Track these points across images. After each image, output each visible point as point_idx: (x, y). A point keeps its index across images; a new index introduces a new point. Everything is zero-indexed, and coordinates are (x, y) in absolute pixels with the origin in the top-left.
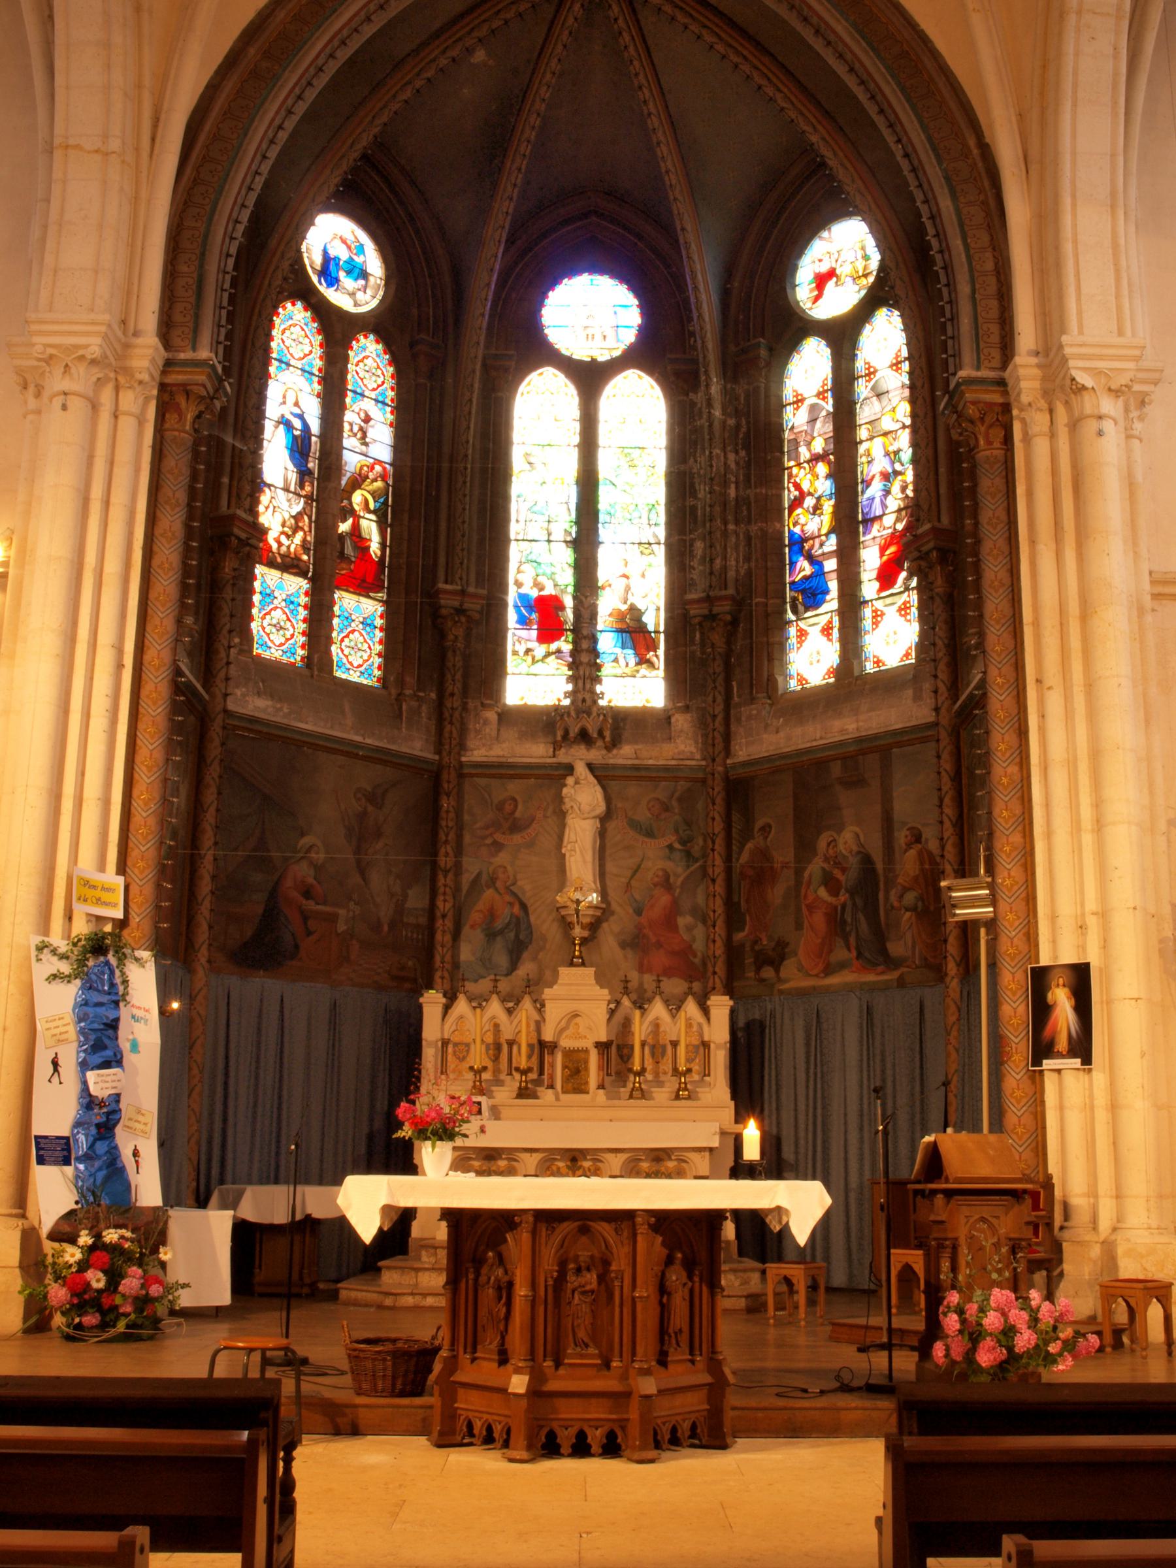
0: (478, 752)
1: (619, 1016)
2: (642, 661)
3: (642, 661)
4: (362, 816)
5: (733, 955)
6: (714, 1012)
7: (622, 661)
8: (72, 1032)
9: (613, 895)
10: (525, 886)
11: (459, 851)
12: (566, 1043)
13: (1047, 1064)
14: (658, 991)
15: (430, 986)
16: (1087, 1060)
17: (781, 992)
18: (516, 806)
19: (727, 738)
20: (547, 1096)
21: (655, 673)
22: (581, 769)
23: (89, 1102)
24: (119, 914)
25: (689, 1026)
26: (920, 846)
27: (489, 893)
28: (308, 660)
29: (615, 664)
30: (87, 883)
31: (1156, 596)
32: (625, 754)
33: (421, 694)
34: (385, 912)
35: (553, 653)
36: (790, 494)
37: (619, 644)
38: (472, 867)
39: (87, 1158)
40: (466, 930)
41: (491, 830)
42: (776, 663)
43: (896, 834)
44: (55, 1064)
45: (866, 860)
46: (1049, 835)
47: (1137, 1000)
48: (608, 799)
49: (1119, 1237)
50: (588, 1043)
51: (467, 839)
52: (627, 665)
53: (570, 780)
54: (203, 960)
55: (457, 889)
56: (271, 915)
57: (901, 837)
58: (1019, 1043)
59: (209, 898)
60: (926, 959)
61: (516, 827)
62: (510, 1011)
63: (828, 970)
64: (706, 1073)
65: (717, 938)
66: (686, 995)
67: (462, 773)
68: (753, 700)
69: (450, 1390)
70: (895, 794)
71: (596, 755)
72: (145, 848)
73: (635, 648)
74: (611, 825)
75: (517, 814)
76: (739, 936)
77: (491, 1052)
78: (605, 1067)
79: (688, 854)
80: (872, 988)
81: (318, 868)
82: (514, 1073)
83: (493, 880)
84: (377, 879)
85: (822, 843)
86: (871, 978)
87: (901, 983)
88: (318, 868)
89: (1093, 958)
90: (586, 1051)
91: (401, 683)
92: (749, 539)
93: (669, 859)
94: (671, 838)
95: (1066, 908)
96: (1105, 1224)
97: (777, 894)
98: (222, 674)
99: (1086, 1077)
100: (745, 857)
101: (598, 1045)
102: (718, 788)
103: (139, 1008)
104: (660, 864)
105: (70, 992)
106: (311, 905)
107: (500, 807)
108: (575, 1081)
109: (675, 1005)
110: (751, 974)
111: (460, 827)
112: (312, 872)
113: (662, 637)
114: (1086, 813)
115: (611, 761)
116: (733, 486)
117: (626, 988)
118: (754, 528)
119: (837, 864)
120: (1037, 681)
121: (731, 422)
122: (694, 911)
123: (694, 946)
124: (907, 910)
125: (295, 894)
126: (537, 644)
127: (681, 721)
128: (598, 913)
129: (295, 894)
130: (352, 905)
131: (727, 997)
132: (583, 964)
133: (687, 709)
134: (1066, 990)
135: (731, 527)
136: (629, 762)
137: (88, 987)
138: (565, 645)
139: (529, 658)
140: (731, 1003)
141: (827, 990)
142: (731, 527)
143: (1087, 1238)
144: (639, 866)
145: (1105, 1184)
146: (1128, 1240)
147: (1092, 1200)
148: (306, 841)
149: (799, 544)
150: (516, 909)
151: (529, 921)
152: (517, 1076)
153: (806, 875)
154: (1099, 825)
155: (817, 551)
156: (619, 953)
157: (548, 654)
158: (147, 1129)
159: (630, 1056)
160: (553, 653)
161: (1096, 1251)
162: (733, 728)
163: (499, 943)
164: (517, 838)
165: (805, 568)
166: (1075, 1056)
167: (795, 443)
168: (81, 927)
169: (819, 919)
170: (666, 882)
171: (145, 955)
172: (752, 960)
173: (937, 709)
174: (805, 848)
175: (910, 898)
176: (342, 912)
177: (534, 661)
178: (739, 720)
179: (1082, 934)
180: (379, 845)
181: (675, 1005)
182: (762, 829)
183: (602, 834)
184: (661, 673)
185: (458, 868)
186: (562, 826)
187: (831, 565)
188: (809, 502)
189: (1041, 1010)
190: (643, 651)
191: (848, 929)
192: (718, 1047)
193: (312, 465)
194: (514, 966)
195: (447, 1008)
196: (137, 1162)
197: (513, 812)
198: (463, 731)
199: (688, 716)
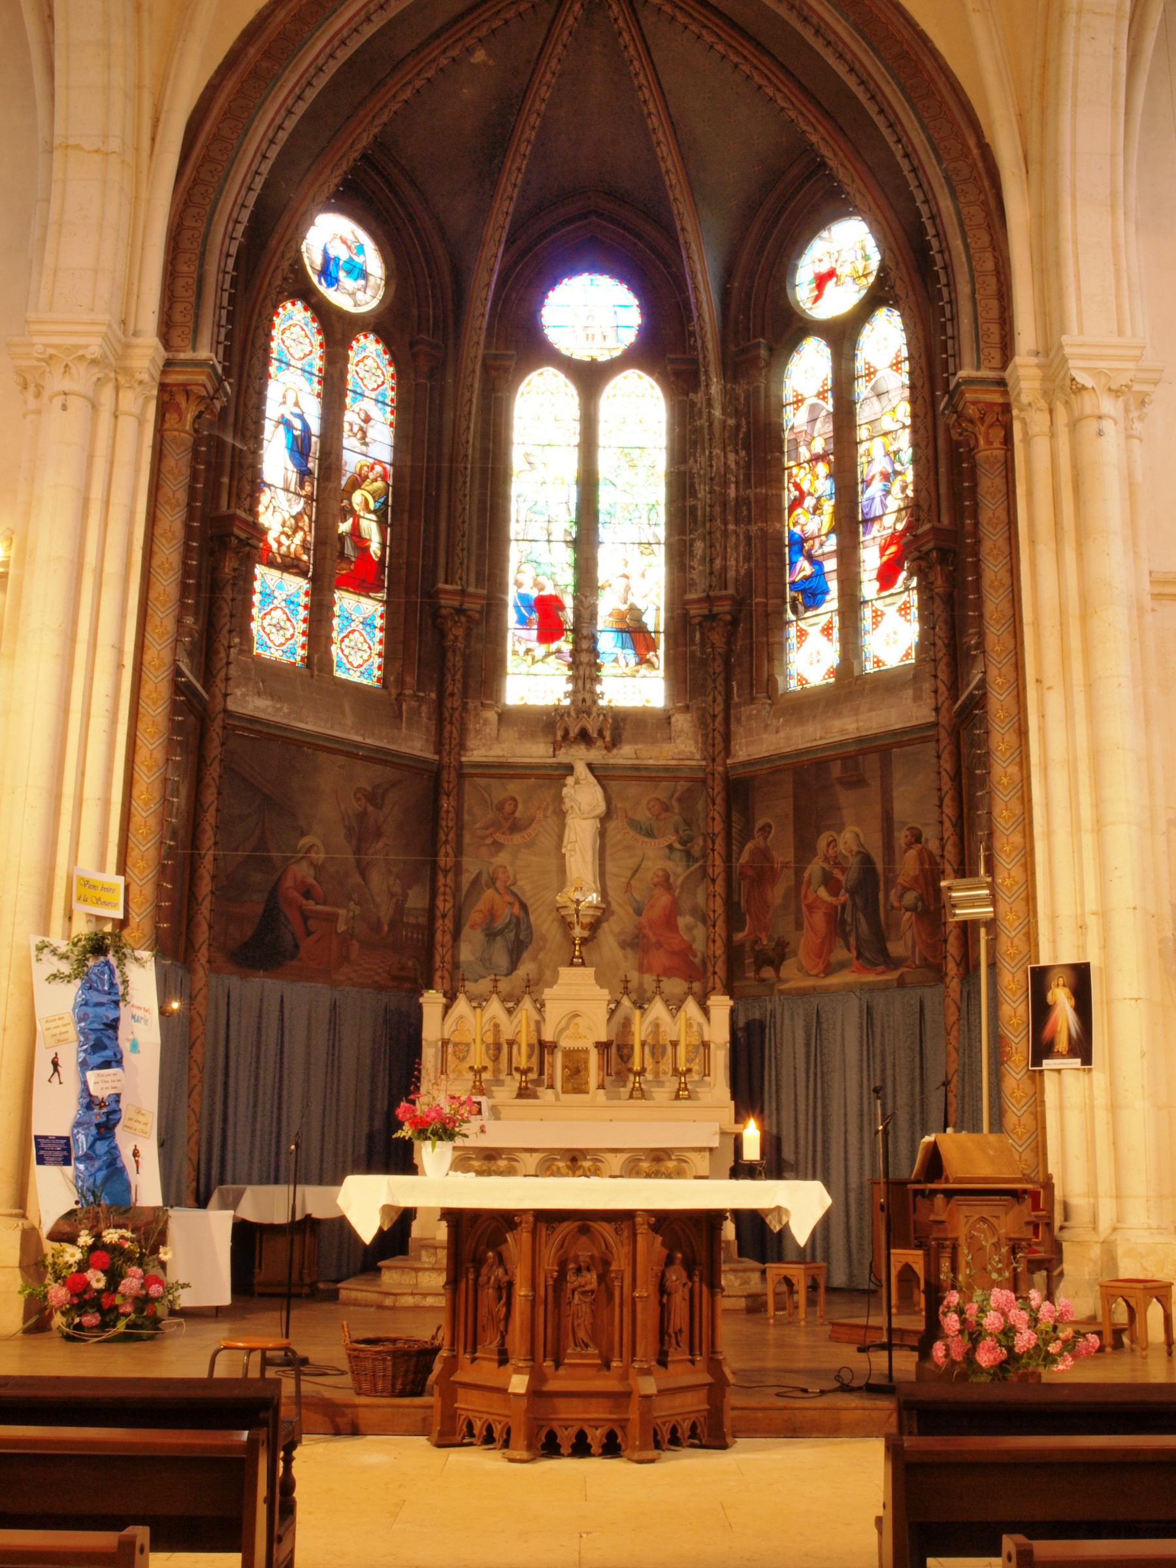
0: (478, 752)
1: (619, 1016)
2: (643, 661)
3: (643, 661)
4: (362, 816)
5: (734, 955)
6: (714, 1012)
7: (622, 662)
8: (72, 1031)
9: (612, 894)
10: (525, 887)
11: (459, 851)
12: (566, 1043)
13: (1047, 1064)
14: (658, 991)
15: (430, 986)
16: (1087, 1060)
17: (781, 992)
18: (516, 806)
19: (727, 738)
20: (547, 1095)
21: (655, 673)
22: (581, 770)
23: (90, 1102)
24: (119, 914)
25: (689, 1025)
26: (919, 846)
27: (489, 893)
28: (308, 661)
29: (614, 664)
30: (87, 883)
31: (1156, 596)
32: (625, 754)
33: (422, 694)
34: (385, 913)
35: (553, 653)
36: (789, 494)
37: (619, 644)
38: (471, 867)
39: (87, 1158)
40: (466, 930)
41: (491, 830)
42: (776, 663)
43: (896, 834)
44: (55, 1064)
45: (866, 860)
46: (1049, 834)
47: (1137, 1000)
48: (608, 800)
49: (1118, 1237)
50: (588, 1043)
51: (467, 838)
52: (627, 665)
53: (570, 780)
54: (203, 960)
55: (457, 889)
56: (271, 914)
57: (901, 837)
58: (1019, 1043)
59: (208, 898)
60: (926, 959)
61: (516, 827)
62: (510, 1011)
63: (829, 970)
64: (706, 1073)
65: (717, 938)
66: (686, 994)
67: (462, 773)
68: (752, 700)
69: (450, 1391)
70: (895, 794)
71: (596, 755)
72: (145, 849)
73: (635, 648)
74: (612, 825)
75: (517, 814)
76: (739, 936)
77: (491, 1052)
78: (605, 1067)
79: (689, 856)
80: (872, 988)
81: (318, 868)
82: (514, 1072)
83: (493, 881)
84: (376, 879)
85: (822, 843)
86: (871, 978)
87: (901, 983)
88: (318, 868)
89: (1093, 958)
90: (586, 1051)
91: (401, 683)
92: (749, 539)
93: (670, 859)
94: (671, 838)
95: (1066, 907)
96: (1105, 1223)
97: (777, 894)
98: (222, 674)
99: (1086, 1077)
100: (745, 857)
101: (600, 1045)
102: (718, 788)
103: (139, 1008)
104: (661, 864)
105: (71, 992)
106: (310, 905)
107: (500, 807)
108: (575, 1080)
109: (675, 1005)
110: (751, 974)
111: (460, 828)
112: (312, 872)
113: (662, 637)
114: (1086, 813)
115: (611, 761)
116: (733, 486)
117: (626, 988)
118: (754, 529)
119: (837, 864)
120: (1037, 681)
121: (731, 422)
122: (694, 911)
123: (694, 946)
124: (907, 910)
125: (295, 894)
126: (537, 644)
127: (682, 722)
128: (599, 913)
129: (295, 894)
130: (352, 905)
131: (727, 997)
132: (583, 964)
133: (687, 709)
134: (1067, 990)
135: (731, 527)
136: (630, 762)
137: (89, 987)
138: (565, 645)
139: (529, 658)
140: (731, 1003)
141: (827, 990)
142: (731, 527)
143: (1087, 1238)
144: (639, 866)
145: (1105, 1186)
146: (1128, 1240)
147: (1092, 1200)
148: (306, 841)
149: (799, 543)
150: (516, 909)
151: (528, 920)
152: (517, 1076)
153: (806, 875)
154: (1099, 825)
155: (816, 551)
156: (619, 953)
157: (548, 654)
158: (147, 1129)
159: (630, 1056)
160: (553, 653)
161: (1096, 1251)
162: (733, 727)
163: (499, 943)
164: (517, 838)
165: (804, 568)
166: (1075, 1056)
167: (795, 443)
168: (82, 928)
169: (819, 919)
170: (666, 882)
171: (146, 955)
172: (752, 960)
173: (937, 710)
174: (805, 848)
175: (910, 898)
176: (342, 912)
177: (534, 661)
178: (739, 720)
179: (1082, 934)
180: (379, 845)
181: (675, 1005)
182: (762, 829)
183: (602, 833)
184: (661, 672)
185: (458, 869)
186: (562, 826)
187: (831, 565)
188: (809, 502)
189: (1041, 1010)
190: (644, 652)
191: (848, 929)
192: (718, 1047)
193: (313, 465)
194: (514, 965)
195: (447, 1008)
196: (137, 1162)
197: (513, 812)
198: (463, 731)
199: (688, 716)
